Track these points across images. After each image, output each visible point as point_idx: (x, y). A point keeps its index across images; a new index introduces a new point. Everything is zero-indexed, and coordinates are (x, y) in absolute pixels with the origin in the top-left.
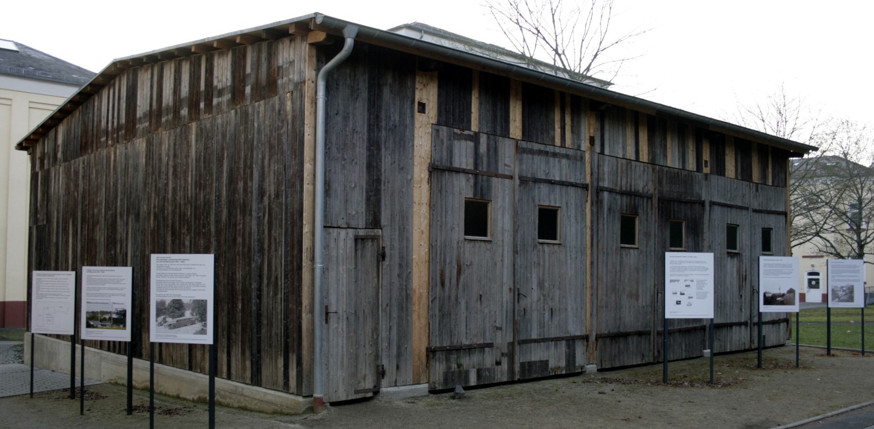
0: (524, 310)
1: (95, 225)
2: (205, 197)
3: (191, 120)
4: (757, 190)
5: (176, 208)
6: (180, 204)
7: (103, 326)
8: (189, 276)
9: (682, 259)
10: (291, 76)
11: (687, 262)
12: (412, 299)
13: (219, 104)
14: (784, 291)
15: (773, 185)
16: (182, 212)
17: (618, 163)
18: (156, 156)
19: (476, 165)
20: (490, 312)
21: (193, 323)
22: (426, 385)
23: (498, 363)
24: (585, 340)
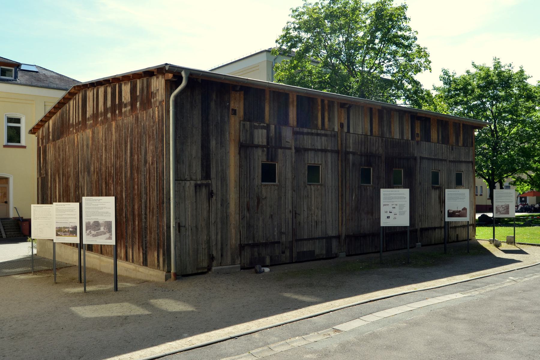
0: (299, 222)
1: (69, 177)
2: (120, 163)
3: (112, 120)
4: (452, 149)
5: (106, 169)
6: (108, 167)
7: (65, 235)
8: (102, 208)
9: (390, 192)
10: (157, 98)
11: (393, 194)
13: (125, 112)
14: (460, 209)
15: (463, 145)
16: (109, 171)
17: (359, 137)
18: (96, 140)
20: (278, 224)
21: (105, 234)
22: (239, 265)
23: (283, 252)
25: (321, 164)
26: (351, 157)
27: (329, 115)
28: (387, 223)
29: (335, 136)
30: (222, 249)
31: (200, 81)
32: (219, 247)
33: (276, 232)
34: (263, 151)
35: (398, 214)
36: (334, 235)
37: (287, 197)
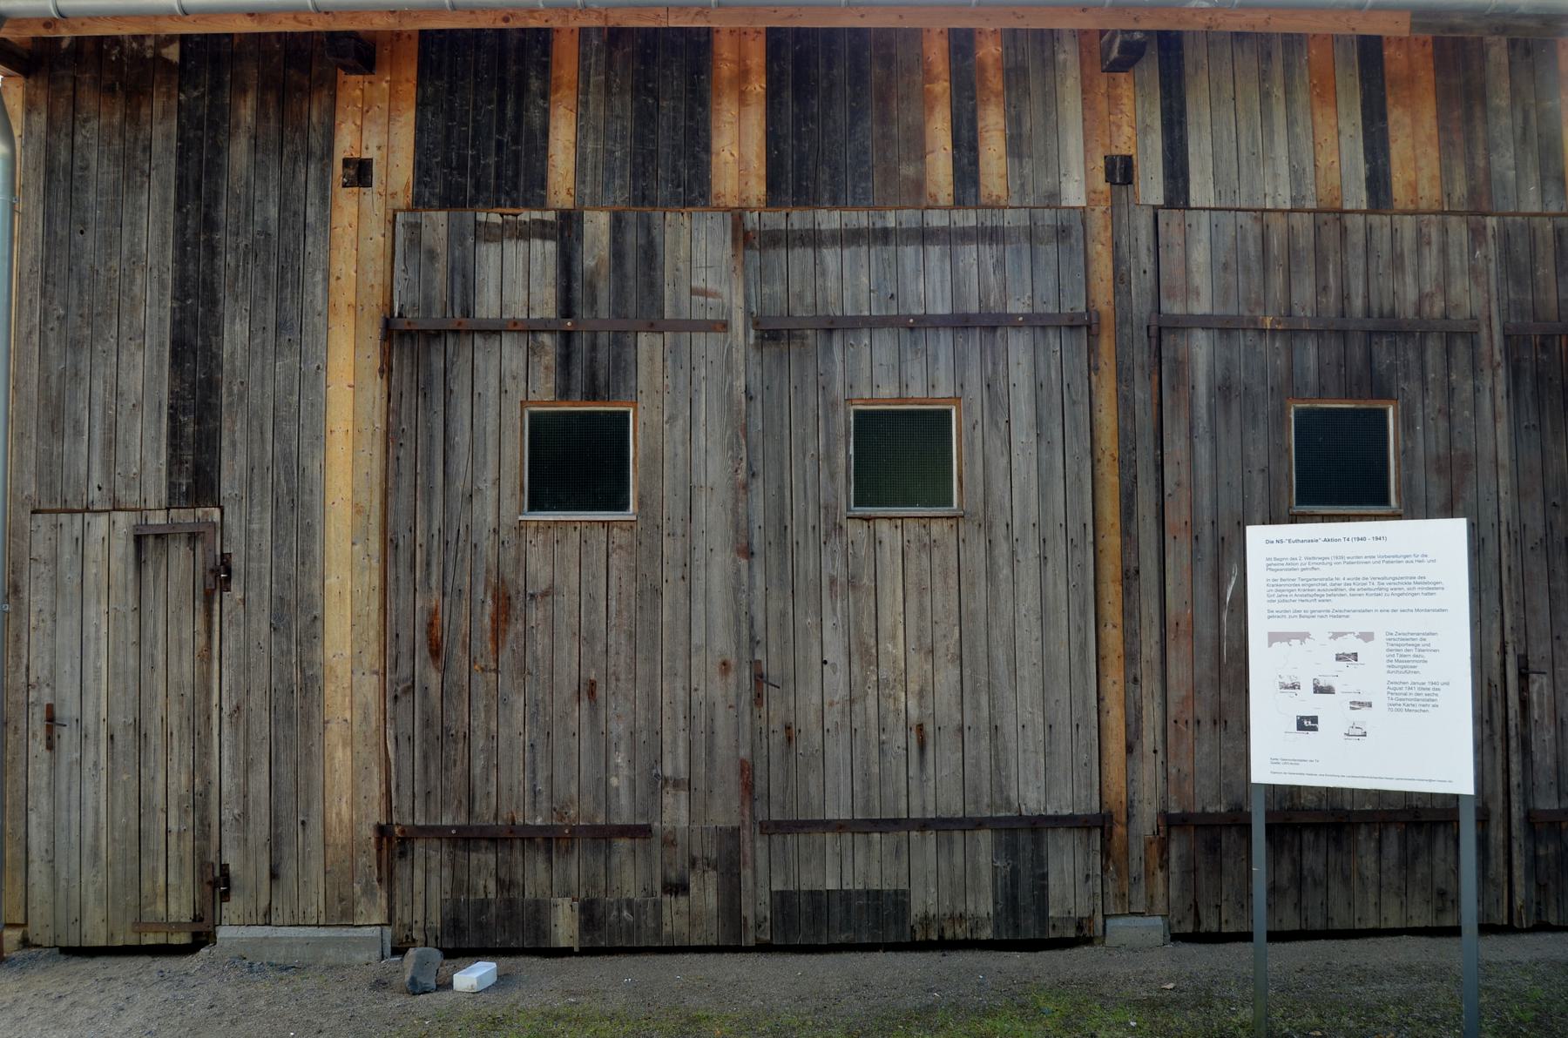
12: (321, 690)
19: (567, 307)
23: (678, 888)
24: (1097, 833)
25: (956, 399)
26: (1201, 349)
27: (1014, 122)
28: (1295, 762)
29: (1062, 233)
30: (275, 843)
31: (173, 53)
32: (260, 828)
33: (625, 771)
34: (532, 351)
35: (1380, 700)
36: (1066, 812)
37: (698, 588)
